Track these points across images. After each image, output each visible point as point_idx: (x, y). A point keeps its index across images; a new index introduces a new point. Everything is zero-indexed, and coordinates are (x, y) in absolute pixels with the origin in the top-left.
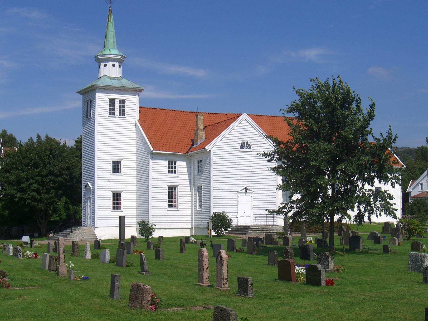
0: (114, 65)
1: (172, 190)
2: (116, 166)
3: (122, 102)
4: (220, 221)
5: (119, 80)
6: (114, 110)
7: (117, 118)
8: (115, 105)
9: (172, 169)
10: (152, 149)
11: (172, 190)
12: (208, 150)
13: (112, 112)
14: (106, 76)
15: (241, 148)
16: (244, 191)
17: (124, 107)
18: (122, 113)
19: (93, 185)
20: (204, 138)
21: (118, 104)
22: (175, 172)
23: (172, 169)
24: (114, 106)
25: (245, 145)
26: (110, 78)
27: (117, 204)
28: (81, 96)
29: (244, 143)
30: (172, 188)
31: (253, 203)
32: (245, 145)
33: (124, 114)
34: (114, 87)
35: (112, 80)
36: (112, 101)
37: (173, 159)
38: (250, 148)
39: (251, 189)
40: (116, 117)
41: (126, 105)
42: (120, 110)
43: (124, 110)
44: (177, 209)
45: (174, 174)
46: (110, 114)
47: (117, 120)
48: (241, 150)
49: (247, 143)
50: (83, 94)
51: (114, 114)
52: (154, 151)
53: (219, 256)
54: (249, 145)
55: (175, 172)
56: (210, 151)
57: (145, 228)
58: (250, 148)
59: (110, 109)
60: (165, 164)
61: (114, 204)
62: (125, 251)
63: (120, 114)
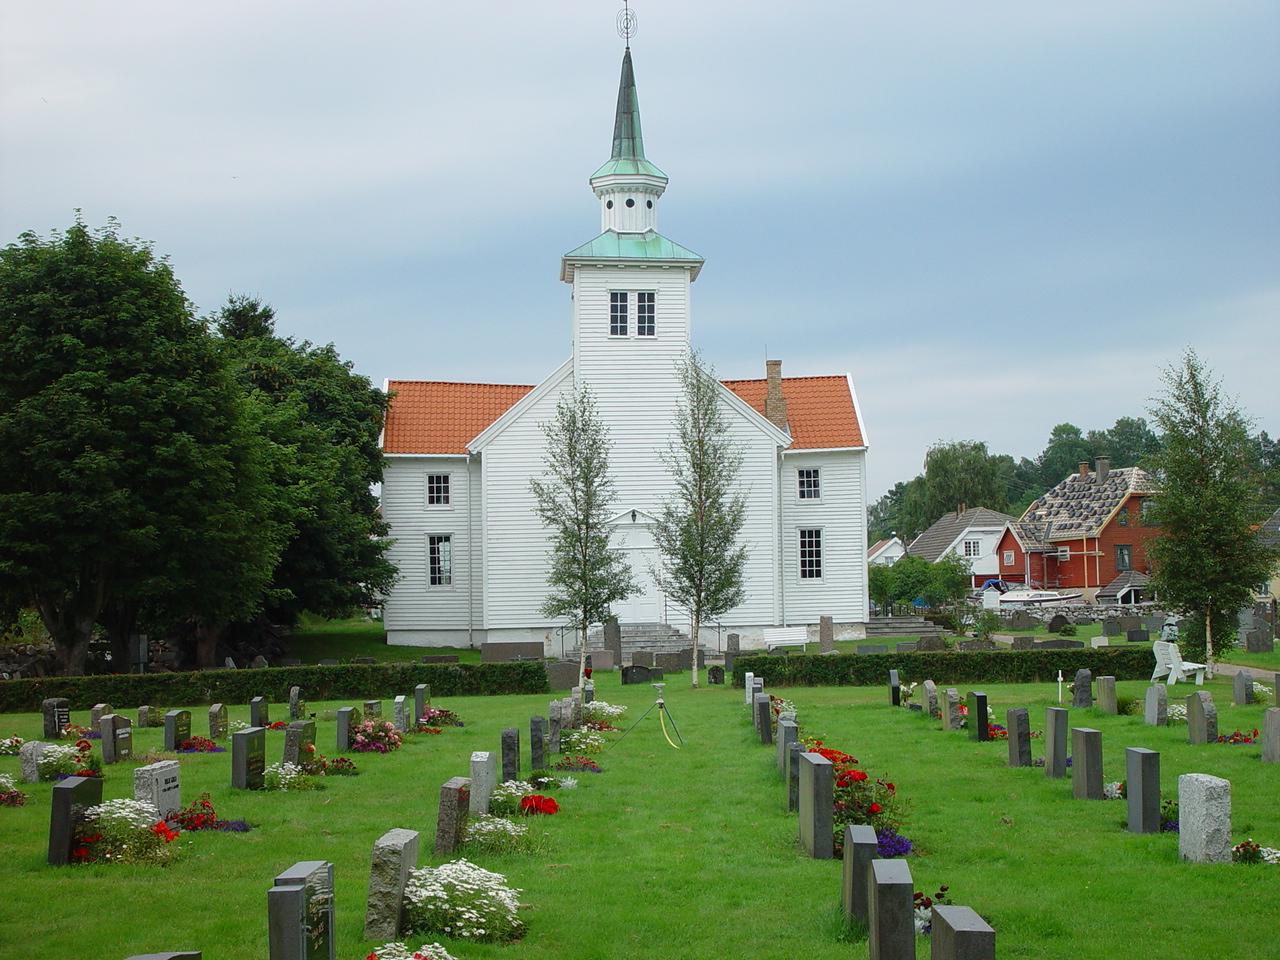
3: (647, 299)
6: (624, 319)
13: (618, 326)
18: (647, 327)
24: (624, 309)
33: (651, 331)
36: (618, 298)
43: (651, 320)
46: (614, 331)
51: (624, 331)
63: (641, 331)
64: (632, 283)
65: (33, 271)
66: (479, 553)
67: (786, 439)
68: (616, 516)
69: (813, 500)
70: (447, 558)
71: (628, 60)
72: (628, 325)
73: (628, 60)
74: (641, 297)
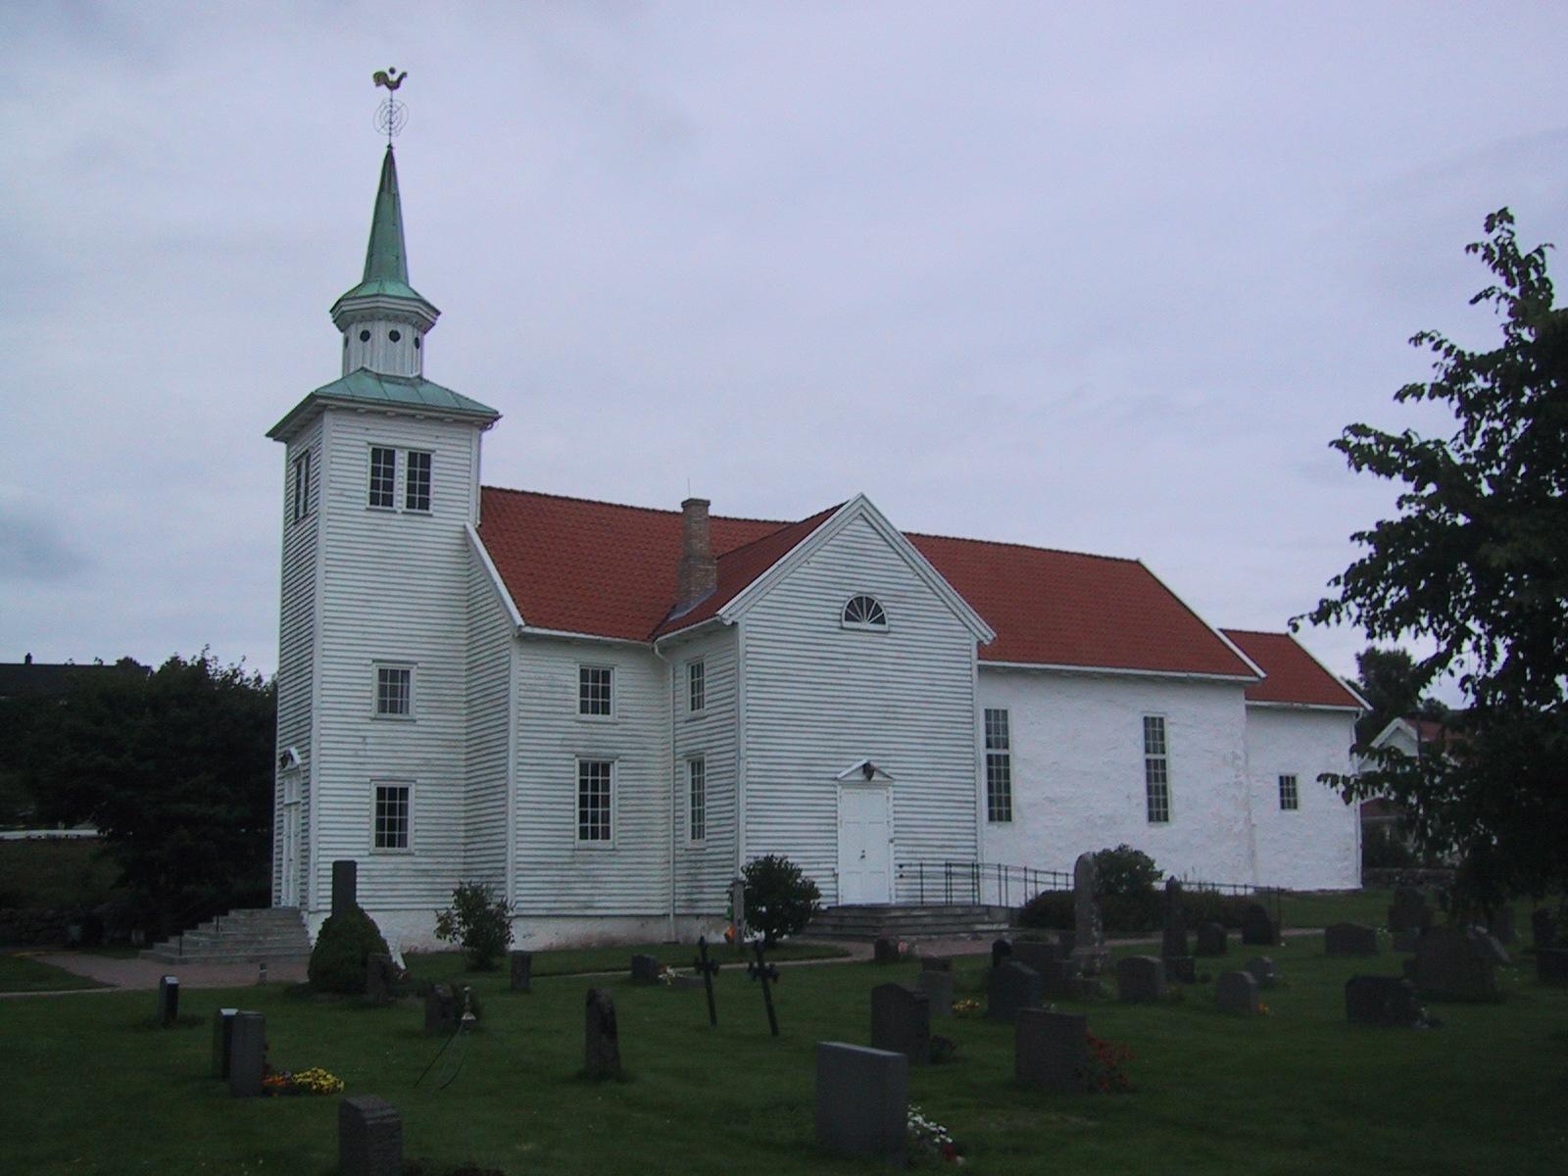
0: (395, 336)
1: (594, 779)
2: (392, 690)
3: (420, 462)
4: (776, 894)
5: (412, 385)
6: (389, 486)
7: (402, 517)
8: (392, 471)
9: (596, 693)
10: (520, 621)
11: (594, 779)
12: (728, 623)
13: (381, 496)
14: (366, 370)
15: (848, 618)
16: (860, 777)
17: (426, 477)
18: (419, 500)
19: (306, 754)
20: (712, 585)
21: (405, 468)
22: (606, 710)
23: (596, 693)
24: (390, 473)
25: (863, 609)
26: (379, 377)
27: (392, 827)
28: (281, 447)
29: (859, 599)
30: (595, 766)
31: (893, 823)
32: (863, 609)
33: (425, 504)
34: (392, 404)
35: (386, 385)
36: (383, 457)
37: (597, 660)
38: (881, 621)
39: (887, 771)
40: (395, 512)
41: (433, 471)
42: (411, 489)
43: (426, 490)
44: (406, 717)
45: (600, 717)
46: (374, 500)
47: (398, 521)
48: (847, 624)
49: (870, 601)
50: (286, 440)
51: (388, 501)
52: (528, 630)
53: (365, 292)
54: (878, 609)
55: (606, 710)
56: (734, 624)
57: (479, 917)
58: (881, 621)
59: (374, 485)
60: (564, 673)
61: (380, 824)
62: (1455, 650)
63: (410, 503)
64: (404, 438)
65: (201, 934)
66: (834, 841)
67: (988, 635)
68: (850, 770)
69: (599, 843)
70: (1051, 878)
71: (389, 161)
72: (406, 482)
73: (389, 161)
74: (412, 457)
